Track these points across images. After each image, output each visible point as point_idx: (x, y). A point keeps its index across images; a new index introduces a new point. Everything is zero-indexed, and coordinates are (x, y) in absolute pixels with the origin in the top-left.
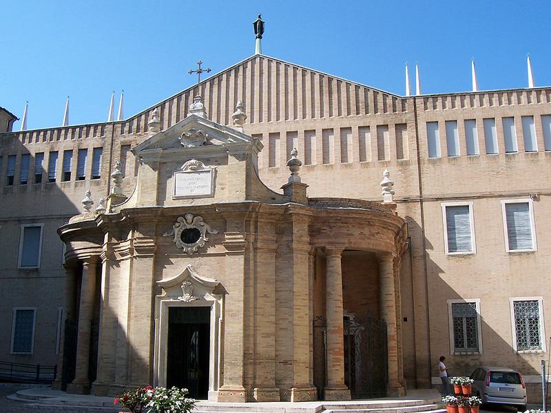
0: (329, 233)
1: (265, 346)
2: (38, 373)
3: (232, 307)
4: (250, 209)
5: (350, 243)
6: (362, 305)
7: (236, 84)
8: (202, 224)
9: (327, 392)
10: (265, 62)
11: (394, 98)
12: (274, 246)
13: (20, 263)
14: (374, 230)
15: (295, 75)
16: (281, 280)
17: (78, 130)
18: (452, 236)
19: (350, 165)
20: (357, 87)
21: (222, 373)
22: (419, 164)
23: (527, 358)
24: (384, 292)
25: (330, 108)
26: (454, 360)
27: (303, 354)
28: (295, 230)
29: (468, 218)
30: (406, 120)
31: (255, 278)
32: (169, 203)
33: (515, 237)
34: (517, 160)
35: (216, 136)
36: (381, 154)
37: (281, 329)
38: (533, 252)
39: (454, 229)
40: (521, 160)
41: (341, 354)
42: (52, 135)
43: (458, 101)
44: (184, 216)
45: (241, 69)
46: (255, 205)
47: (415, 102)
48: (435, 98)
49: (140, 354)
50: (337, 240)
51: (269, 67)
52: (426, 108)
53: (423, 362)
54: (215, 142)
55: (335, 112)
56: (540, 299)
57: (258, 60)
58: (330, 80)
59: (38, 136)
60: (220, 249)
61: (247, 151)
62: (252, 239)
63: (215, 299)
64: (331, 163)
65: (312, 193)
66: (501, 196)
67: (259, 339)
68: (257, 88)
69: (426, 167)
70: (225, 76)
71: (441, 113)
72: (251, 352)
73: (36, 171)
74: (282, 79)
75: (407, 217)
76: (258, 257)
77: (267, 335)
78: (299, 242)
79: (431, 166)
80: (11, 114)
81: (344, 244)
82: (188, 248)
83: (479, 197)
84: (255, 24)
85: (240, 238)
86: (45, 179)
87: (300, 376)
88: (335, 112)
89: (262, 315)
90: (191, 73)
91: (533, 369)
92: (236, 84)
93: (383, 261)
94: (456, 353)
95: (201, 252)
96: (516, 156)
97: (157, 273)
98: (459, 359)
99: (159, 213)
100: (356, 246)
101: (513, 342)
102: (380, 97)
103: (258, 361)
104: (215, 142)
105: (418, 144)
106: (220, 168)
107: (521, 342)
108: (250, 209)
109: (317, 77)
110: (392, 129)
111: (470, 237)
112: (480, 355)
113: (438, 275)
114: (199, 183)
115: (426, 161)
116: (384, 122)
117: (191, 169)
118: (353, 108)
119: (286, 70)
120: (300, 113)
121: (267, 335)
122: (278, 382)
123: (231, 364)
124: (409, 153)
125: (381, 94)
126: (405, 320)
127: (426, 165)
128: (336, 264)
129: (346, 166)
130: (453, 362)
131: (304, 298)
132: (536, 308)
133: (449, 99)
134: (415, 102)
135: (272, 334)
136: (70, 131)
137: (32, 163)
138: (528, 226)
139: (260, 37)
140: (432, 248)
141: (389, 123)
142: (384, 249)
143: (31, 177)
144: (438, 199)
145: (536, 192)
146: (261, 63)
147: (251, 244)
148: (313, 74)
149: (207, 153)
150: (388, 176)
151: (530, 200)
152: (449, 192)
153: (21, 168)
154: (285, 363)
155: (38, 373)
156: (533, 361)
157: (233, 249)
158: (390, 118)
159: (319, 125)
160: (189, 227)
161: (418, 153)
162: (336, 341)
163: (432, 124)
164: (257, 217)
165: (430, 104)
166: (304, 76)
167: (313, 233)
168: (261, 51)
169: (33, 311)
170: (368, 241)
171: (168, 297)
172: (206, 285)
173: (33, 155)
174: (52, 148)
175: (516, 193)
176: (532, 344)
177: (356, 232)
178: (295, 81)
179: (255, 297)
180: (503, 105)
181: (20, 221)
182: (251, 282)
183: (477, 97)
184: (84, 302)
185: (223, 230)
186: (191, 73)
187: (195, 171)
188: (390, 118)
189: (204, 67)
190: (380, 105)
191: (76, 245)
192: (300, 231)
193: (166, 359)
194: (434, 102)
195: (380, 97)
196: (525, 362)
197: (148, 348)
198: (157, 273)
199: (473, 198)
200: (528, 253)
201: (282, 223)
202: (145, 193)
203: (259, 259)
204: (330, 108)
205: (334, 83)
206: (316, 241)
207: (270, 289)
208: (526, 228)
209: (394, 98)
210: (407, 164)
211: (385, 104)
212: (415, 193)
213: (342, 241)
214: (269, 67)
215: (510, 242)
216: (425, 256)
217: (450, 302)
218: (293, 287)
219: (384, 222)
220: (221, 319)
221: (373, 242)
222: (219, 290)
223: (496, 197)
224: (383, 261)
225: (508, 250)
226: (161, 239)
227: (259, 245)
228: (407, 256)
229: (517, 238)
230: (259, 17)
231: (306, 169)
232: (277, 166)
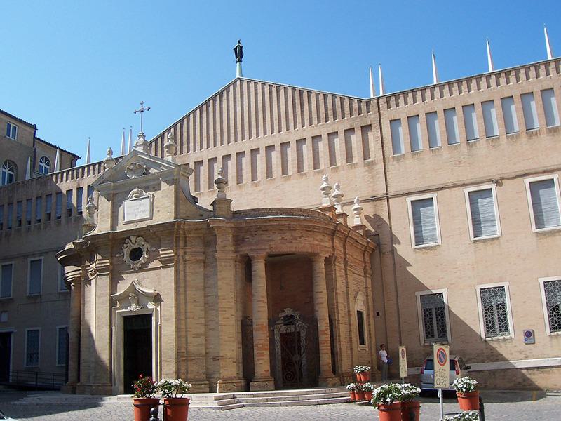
0: (251, 241)
1: (196, 345)
2: (37, 378)
4: (176, 227)
5: (271, 248)
7: (221, 108)
8: (143, 243)
9: (251, 383)
10: (245, 84)
11: (359, 102)
12: (201, 257)
13: (28, 291)
14: (296, 234)
15: (271, 93)
16: (208, 287)
17: (97, 166)
18: (419, 229)
20: (325, 96)
21: (161, 370)
22: (384, 163)
23: (495, 345)
24: (316, 290)
25: (303, 119)
26: (424, 350)
27: (230, 349)
28: (219, 241)
29: (433, 210)
30: (371, 121)
31: (185, 287)
32: (121, 228)
33: (481, 224)
34: (478, 147)
35: (153, 166)
36: (349, 157)
37: (210, 329)
38: (498, 238)
39: (421, 222)
40: (482, 146)
41: (265, 349)
42: (72, 174)
43: (532, 72)
44: (129, 238)
45: (225, 93)
46: (180, 223)
47: (378, 103)
48: (397, 95)
49: (536, 383)
50: (258, 247)
51: (249, 88)
52: (389, 107)
54: (153, 171)
55: (307, 122)
56: (506, 285)
57: (238, 82)
58: (301, 92)
59: (67, 175)
60: (157, 264)
61: (178, 177)
62: (181, 252)
63: (154, 307)
64: (305, 172)
65: (235, 207)
66: (464, 185)
67: (190, 339)
68: (239, 109)
69: (392, 165)
70: (211, 102)
71: (402, 110)
72: (183, 350)
73: (67, 206)
74: (267, 96)
75: (374, 215)
76: (187, 267)
77: (198, 336)
78: (223, 251)
80: (72, 154)
81: (266, 249)
82: (137, 265)
83: (442, 189)
84: (236, 49)
85: (170, 253)
86: (74, 212)
88: (307, 122)
89: (193, 318)
91: (502, 355)
92: (221, 108)
93: (313, 261)
94: (426, 344)
95: (144, 268)
96: (477, 143)
97: (113, 288)
99: (111, 237)
100: (277, 251)
101: (481, 330)
102: (346, 103)
103: (189, 359)
104: (153, 171)
105: (382, 143)
106: (158, 194)
107: (490, 329)
108: (176, 227)
109: (290, 91)
110: (358, 132)
111: (435, 229)
113: (405, 268)
116: (351, 125)
118: (323, 116)
119: (263, 89)
120: (276, 128)
121: (198, 336)
122: (209, 377)
124: (375, 154)
125: (347, 99)
126: (378, 314)
127: (391, 163)
128: (260, 269)
129: (318, 172)
130: (423, 353)
132: (503, 294)
133: (410, 95)
134: (378, 103)
136: (91, 167)
137: (64, 200)
138: (493, 212)
139: (240, 61)
140: (399, 243)
141: (355, 126)
142: (310, 251)
143: (63, 212)
144: (403, 195)
145: (498, 177)
146: (241, 85)
147: (181, 258)
148: (286, 88)
149: (147, 181)
150: (326, 180)
151: (493, 186)
152: (413, 187)
153: (57, 205)
154: (214, 359)
155: (37, 378)
156: (501, 347)
157: (166, 262)
158: (357, 122)
159: (293, 137)
160: (134, 247)
161: (383, 152)
162: (261, 337)
163: (395, 122)
164: (185, 234)
165: (393, 103)
166: (278, 91)
167: (239, 243)
168: (241, 74)
169: (38, 330)
170: (289, 245)
171: (122, 308)
172: (146, 295)
173: (65, 192)
174: (79, 184)
175: (478, 180)
176: (501, 331)
177: (277, 237)
178: (271, 98)
179: (186, 303)
180: (541, 77)
181: (26, 256)
182: (182, 290)
183: (437, 89)
184: (72, 317)
185: (159, 247)
187: (138, 198)
188: (357, 122)
189: (145, 106)
190: (347, 110)
191: (67, 269)
192: (224, 243)
193: (122, 361)
194: (396, 100)
195: (346, 103)
196: (492, 349)
197: (107, 352)
198: (113, 288)
199: (437, 190)
200: (492, 239)
201: (207, 237)
202: (103, 221)
203: (188, 270)
204: (303, 119)
205: (305, 94)
206: (241, 249)
207: (199, 295)
208: (490, 214)
209: (359, 102)
210: (373, 163)
211: (351, 108)
212: (381, 191)
213: (263, 247)
214: (249, 88)
215: (474, 230)
216: (393, 251)
217: (418, 294)
218: (217, 292)
219: (308, 226)
220: (159, 323)
221: (294, 245)
222: (157, 299)
223: (458, 186)
224: (313, 261)
225: (472, 238)
226: (115, 259)
227: (187, 257)
228: (377, 251)
229: (482, 225)
230: (239, 42)
231: (283, 180)
232: (259, 180)
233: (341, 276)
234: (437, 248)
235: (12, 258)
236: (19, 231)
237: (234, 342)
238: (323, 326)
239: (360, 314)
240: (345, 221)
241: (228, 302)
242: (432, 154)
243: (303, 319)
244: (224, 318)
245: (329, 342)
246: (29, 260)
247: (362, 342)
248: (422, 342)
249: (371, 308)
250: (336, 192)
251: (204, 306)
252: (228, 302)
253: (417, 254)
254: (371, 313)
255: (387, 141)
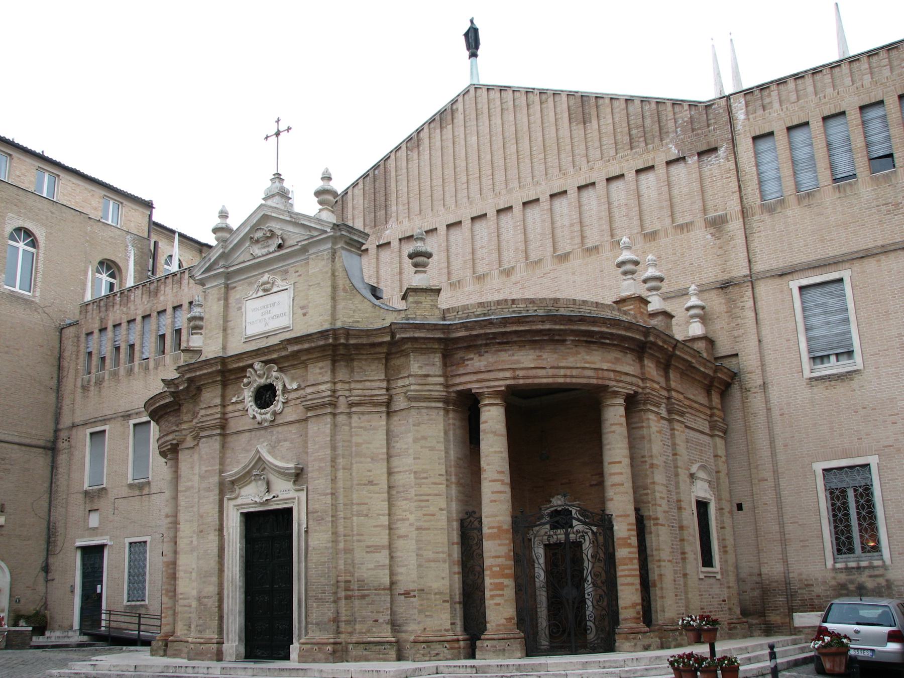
2: (139, 624)
3: (317, 506)
6: (591, 486)
9: (478, 643)
19: (283, 239)
26: (834, 578)
53: (775, 585)
79: (766, 216)
87: (431, 616)
90: (267, 138)
98: (842, 577)
112: (884, 567)
114: (275, 311)
115: (758, 211)
117: (265, 290)
123: (317, 599)
126: (740, 507)
127: (756, 218)
131: (437, 481)
135: (383, 547)
155: (139, 624)
160: (262, 381)
161: (741, 198)
169: (145, 542)
186: (267, 138)
212: (740, 269)
233: (659, 432)
234: (857, 377)
235: (105, 420)
236: (115, 374)
237: (445, 561)
238: (623, 529)
239: (702, 506)
240: (669, 326)
241: (435, 483)
242: (837, 195)
243: (587, 517)
244: (425, 515)
245: (636, 561)
246: (132, 422)
247: (707, 560)
248: (830, 563)
249: (725, 495)
250: (651, 272)
251: (388, 493)
252: (435, 483)
253: (815, 390)
254: (727, 507)
255: (748, 177)
